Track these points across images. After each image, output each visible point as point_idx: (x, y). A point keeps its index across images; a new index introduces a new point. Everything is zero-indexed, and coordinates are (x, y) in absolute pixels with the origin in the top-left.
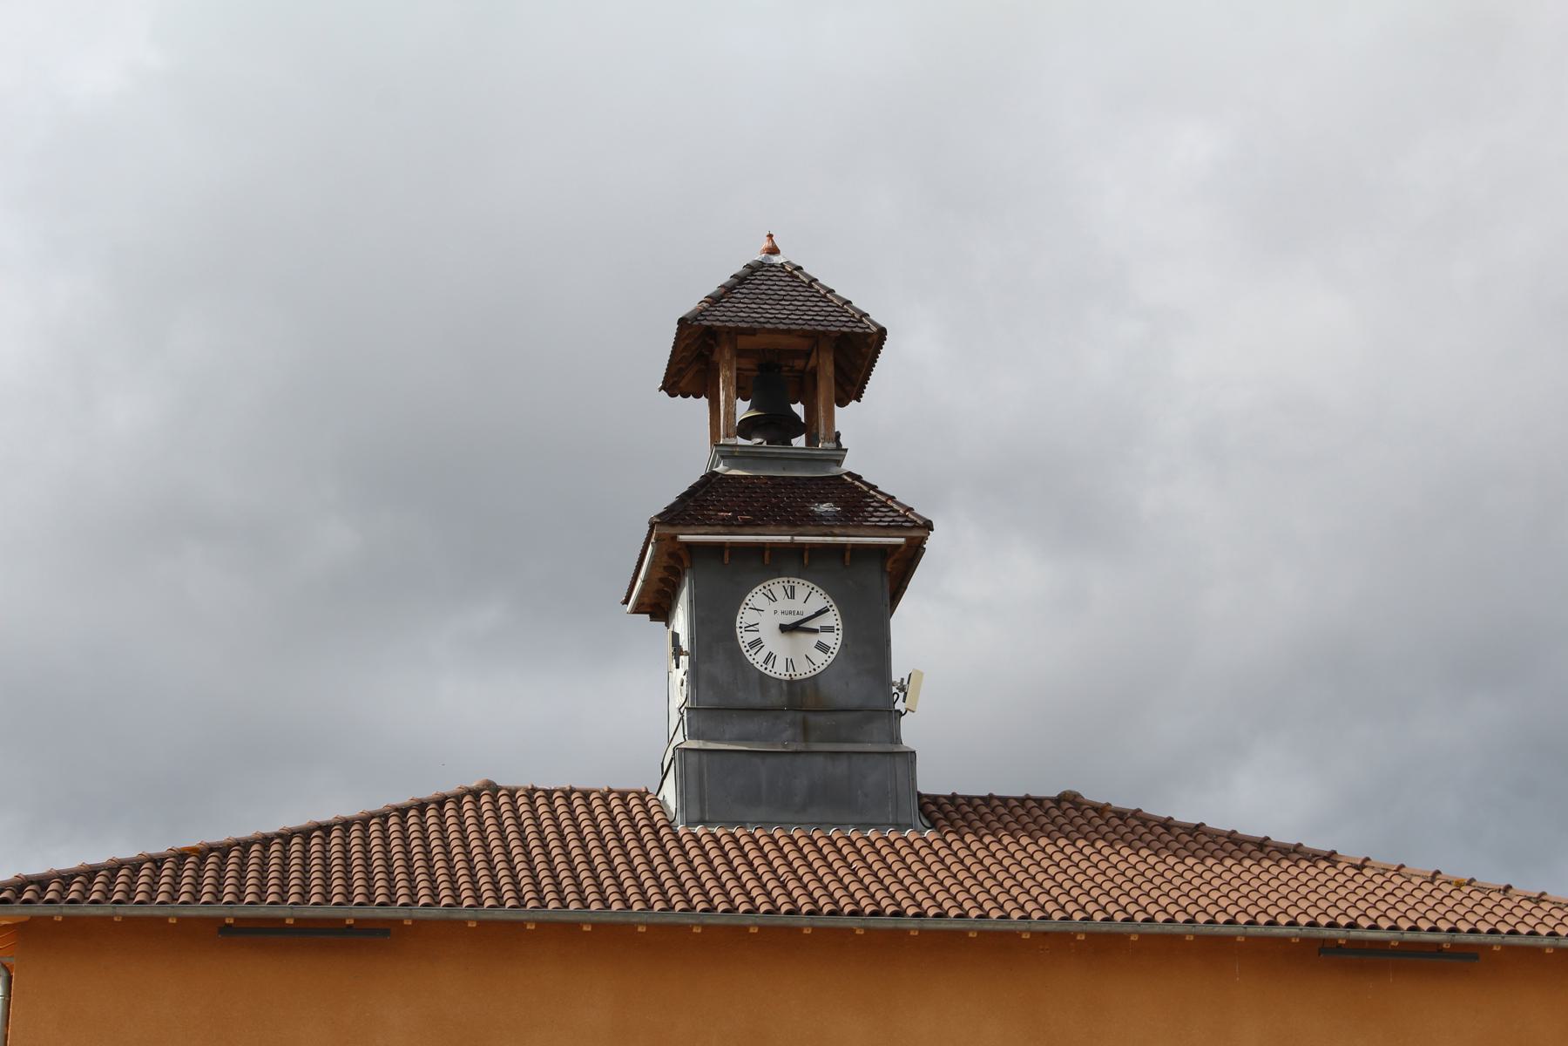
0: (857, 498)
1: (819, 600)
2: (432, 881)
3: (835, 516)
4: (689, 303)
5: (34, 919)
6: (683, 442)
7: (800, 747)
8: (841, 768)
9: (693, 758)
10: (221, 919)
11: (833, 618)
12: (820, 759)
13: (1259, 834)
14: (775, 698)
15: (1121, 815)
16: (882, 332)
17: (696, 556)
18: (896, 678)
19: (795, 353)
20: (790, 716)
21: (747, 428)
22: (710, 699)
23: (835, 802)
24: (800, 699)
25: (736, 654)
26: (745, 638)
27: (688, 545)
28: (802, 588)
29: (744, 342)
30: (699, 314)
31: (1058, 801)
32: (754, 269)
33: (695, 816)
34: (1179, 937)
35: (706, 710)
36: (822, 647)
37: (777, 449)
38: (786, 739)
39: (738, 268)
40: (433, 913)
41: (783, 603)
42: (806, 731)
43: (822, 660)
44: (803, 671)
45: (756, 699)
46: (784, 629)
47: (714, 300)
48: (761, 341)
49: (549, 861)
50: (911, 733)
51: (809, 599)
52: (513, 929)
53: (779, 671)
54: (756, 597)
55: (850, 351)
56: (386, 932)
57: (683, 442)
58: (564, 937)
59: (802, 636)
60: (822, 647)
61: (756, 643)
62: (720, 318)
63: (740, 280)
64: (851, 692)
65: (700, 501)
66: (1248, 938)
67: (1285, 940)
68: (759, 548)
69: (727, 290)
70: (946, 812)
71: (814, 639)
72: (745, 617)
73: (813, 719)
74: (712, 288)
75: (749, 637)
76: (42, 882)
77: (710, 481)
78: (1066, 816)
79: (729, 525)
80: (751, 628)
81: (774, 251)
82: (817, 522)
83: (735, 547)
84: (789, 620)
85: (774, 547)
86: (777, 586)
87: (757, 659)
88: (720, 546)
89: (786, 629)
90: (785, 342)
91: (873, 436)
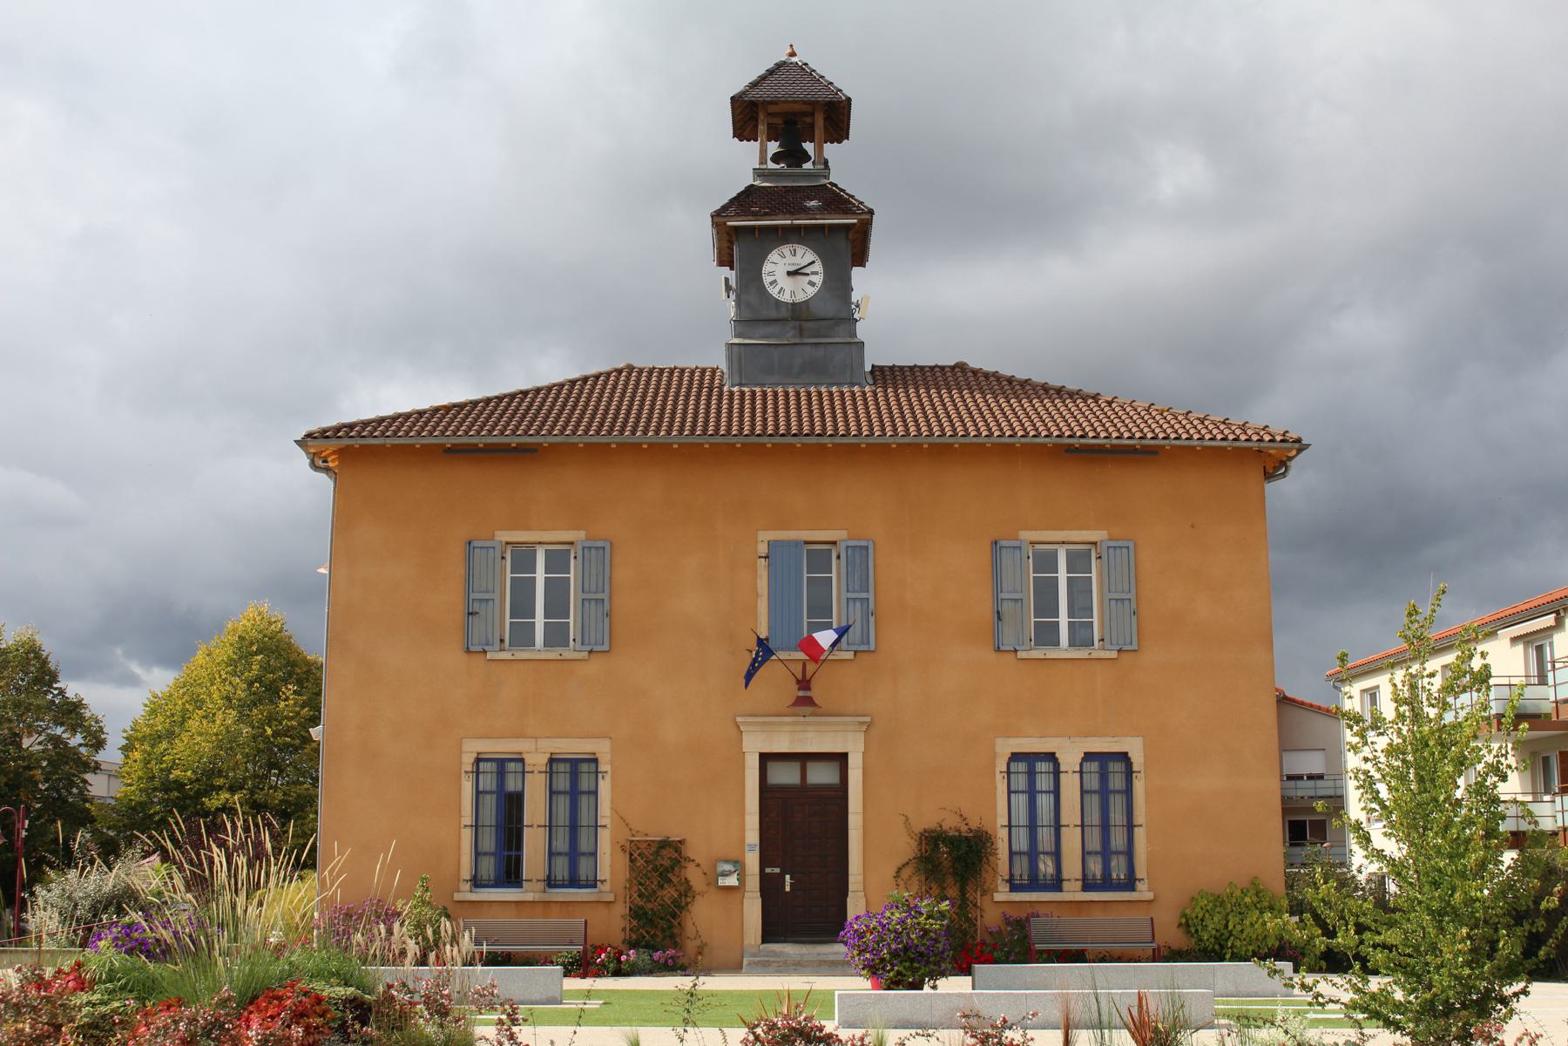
0: (837, 201)
1: (810, 256)
2: (870, 421)
3: (818, 208)
4: (738, 87)
5: (348, 447)
6: (744, 163)
7: (797, 341)
8: (820, 352)
9: (736, 349)
10: (443, 445)
11: (818, 267)
12: (808, 348)
13: (1058, 384)
14: (784, 313)
15: (987, 375)
16: (849, 100)
17: (743, 230)
18: (854, 300)
19: (804, 114)
20: (792, 324)
21: (776, 158)
22: (747, 315)
23: (817, 371)
24: (798, 314)
25: (762, 289)
26: (767, 280)
27: (736, 228)
28: (800, 249)
29: (772, 109)
30: (743, 93)
31: (953, 368)
32: (780, 65)
33: (737, 380)
34: (982, 445)
35: (744, 323)
36: (812, 284)
37: (797, 170)
38: (790, 337)
39: (771, 65)
40: (906, 440)
41: (790, 259)
42: (801, 332)
43: (811, 291)
44: (801, 297)
45: (773, 314)
46: (789, 273)
47: (754, 85)
48: (786, 108)
49: (878, 408)
50: (862, 331)
51: (803, 255)
52: (853, 449)
53: (786, 298)
54: (774, 256)
55: (834, 116)
56: (535, 450)
57: (744, 163)
58: (632, 450)
59: (800, 277)
60: (812, 284)
61: (774, 283)
62: (756, 94)
63: (771, 72)
64: (829, 309)
65: (746, 200)
66: (1235, 448)
67: (1044, 445)
68: (776, 228)
69: (763, 78)
70: (884, 375)
71: (807, 279)
72: (767, 267)
73: (806, 325)
74: (754, 77)
75: (771, 279)
76: (351, 426)
77: (750, 191)
78: (959, 377)
79: (756, 216)
80: (771, 273)
81: (793, 54)
82: (806, 212)
83: (761, 228)
84: (792, 269)
85: (784, 227)
86: (786, 249)
87: (774, 291)
88: (753, 227)
89: (790, 274)
90: (797, 108)
91: (845, 165)
